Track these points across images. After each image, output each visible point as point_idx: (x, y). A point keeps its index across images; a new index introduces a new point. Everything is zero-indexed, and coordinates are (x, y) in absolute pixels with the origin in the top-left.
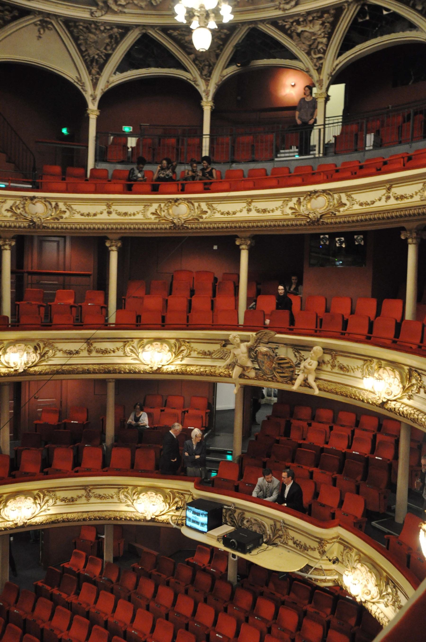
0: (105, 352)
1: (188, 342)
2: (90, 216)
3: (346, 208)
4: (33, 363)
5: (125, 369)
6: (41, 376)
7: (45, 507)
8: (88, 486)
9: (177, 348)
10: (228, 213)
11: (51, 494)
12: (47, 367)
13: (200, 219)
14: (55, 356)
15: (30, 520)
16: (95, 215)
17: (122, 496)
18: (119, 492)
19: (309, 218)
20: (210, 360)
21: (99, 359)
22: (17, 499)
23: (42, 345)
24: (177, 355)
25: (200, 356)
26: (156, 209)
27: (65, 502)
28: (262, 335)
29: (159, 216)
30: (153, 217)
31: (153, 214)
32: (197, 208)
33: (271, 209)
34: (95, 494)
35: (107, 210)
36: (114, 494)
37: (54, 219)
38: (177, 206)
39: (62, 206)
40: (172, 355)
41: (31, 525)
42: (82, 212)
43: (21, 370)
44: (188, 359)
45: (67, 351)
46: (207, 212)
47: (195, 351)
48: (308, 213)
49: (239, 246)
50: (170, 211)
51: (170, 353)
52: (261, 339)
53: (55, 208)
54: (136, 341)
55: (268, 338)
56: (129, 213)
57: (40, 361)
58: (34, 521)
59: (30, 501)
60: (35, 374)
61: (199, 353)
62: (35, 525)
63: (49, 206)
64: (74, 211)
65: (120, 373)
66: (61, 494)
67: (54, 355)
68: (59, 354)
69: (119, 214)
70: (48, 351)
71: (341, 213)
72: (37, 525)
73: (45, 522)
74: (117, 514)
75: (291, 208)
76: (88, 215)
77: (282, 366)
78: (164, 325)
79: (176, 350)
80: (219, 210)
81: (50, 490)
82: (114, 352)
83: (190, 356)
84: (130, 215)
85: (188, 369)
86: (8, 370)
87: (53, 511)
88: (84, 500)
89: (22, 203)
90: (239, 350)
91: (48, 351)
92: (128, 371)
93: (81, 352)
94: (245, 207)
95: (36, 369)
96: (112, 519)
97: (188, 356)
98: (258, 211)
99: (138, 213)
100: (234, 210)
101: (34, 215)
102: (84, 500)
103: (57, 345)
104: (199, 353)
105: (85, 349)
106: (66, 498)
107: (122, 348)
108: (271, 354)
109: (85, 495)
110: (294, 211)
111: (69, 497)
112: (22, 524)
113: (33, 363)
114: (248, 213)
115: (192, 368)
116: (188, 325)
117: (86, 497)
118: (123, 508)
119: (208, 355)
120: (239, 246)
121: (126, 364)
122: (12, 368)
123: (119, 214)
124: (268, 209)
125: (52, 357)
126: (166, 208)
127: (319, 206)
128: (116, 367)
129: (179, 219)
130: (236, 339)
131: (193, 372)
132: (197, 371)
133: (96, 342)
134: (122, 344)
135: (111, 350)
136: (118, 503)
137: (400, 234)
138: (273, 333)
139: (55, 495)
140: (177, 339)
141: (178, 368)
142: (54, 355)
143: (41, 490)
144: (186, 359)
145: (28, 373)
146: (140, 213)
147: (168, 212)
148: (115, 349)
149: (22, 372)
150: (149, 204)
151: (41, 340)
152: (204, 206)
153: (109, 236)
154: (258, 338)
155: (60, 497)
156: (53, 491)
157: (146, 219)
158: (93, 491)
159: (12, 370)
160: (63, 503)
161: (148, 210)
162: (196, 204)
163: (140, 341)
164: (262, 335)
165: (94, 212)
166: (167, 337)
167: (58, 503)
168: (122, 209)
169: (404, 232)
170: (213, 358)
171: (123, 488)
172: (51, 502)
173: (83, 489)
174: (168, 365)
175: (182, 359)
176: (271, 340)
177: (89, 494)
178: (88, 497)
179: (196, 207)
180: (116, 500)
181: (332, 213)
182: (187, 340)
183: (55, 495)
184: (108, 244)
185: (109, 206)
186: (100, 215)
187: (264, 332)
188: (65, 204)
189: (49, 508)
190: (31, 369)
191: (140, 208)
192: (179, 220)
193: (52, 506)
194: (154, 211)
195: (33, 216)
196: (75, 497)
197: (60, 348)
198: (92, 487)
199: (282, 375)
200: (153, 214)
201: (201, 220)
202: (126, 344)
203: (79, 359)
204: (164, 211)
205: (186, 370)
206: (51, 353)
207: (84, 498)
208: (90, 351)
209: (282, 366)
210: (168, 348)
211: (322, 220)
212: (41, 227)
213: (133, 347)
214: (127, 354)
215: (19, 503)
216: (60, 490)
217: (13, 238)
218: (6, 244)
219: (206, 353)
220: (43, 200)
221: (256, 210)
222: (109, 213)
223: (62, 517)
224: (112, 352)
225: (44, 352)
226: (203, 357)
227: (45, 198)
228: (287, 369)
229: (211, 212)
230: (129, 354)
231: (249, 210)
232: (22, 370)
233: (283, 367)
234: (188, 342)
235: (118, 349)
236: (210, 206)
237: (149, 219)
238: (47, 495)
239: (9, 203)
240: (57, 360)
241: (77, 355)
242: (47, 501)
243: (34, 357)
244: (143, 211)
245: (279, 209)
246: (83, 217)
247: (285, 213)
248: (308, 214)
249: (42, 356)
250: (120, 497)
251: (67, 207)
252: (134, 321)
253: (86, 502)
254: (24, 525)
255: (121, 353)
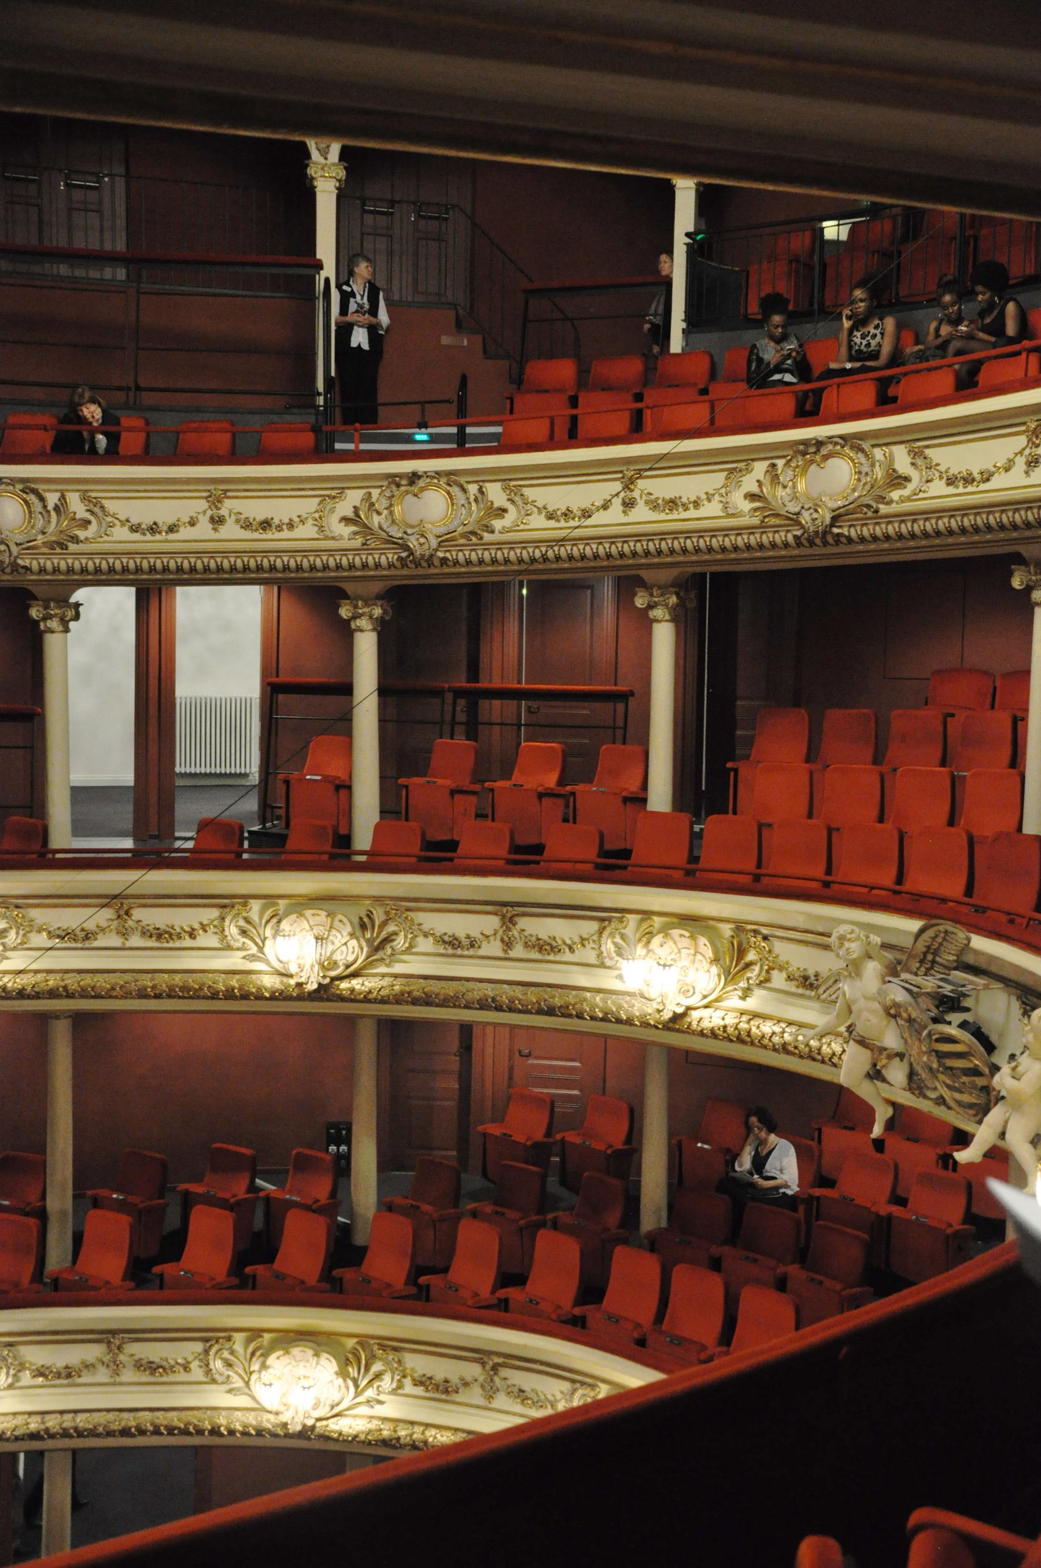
0: (546, 947)
1: (765, 938)
2: (160, 533)
3: (911, 487)
4: (348, 967)
5: (593, 1007)
6: (368, 1005)
7: (370, 1393)
8: (490, 1353)
9: (736, 957)
10: (567, 514)
11: (391, 1357)
12: (387, 981)
13: (485, 534)
14: (414, 950)
15: (324, 1423)
16: (172, 529)
17: (217, 1365)
18: (206, 1352)
19: (800, 524)
20: (816, 1005)
21: (446, 963)
22: (296, 1351)
23: (379, 916)
24: (730, 976)
25: (794, 990)
26: (355, 507)
27: (427, 1390)
28: (936, 936)
29: (366, 530)
30: (347, 530)
31: (346, 520)
32: (476, 500)
33: (693, 498)
34: (509, 1382)
35: (209, 513)
36: (559, 1396)
37: (51, 545)
38: (416, 495)
39: (76, 506)
40: (719, 976)
41: (325, 1438)
42: (134, 521)
43: (312, 986)
44: (764, 992)
45: (446, 938)
46: (505, 511)
47: (781, 969)
48: (797, 510)
49: (348, 622)
50: (397, 510)
51: (714, 970)
52: (935, 953)
53: (57, 509)
54: (255, 905)
55: (954, 949)
56: (276, 521)
57: (369, 964)
58: (335, 1427)
59: (326, 1368)
60: (352, 998)
61: (789, 978)
62: (337, 1440)
63: (37, 506)
64: (109, 519)
65: (580, 1016)
66: (418, 1363)
67: (411, 946)
68: (425, 945)
69: (247, 525)
70: (396, 934)
71: (894, 508)
72: (339, 1439)
73: (362, 1437)
74: (192, 1417)
75: (752, 497)
76: (154, 529)
77: (949, 1063)
78: (691, 876)
79: (731, 961)
80: (540, 504)
81: (393, 1346)
82: (192, 935)
83: (768, 985)
84: (279, 528)
85: (754, 1030)
86: (282, 982)
87: (392, 1408)
88: (475, 1395)
89: (388, 494)
90: (858, 983)
91: (396, 934)
92: (600, 1015)
93: (484, 944)
94: (617, 495)
95: (356, 983)
96: (206, 1433)
97: (764, 982)
98: (654, 505)
99: (303, 522)
100: (586, 504)
101: (412, 527)
102: (475, 1395)
103: (420, 917)
104: (789, 978)
105: (495, 934)
106: (430, 1378)
107: (595, 938)
108: (914, 1015)
109: (481, 1379)
110: (758, 504)
111: (439, 1377)
112: (299, 1428)
113: (348, 967)
114: (624, 512)
115: (767, 1028)
116: (827, 884)
117: (482, 1386)
118: (217, 1397)
119: (811, 987)
120: (348, 622)
121: (599, 991)
122: (291, 976)
123: (247, 525)
124: (684, 500)
125: (404, 952)
126: (385, 503)
127: (835, 481)
128: (571, 997)
129: (423, 536)
130: (847, 944)
131: (766, 1042)
132: (776, 1039)
133: (524, 915)
134: (593, 926)
135: (564, 943)
136: (205, 1383)
137: (1010, 574)
138: (961, 934)
139: (399, 1362)
140: (739, 927)
141: (731, 1020)
142: (411, 946)
143: (363, 1340)
144: (759, 993)
145: (334, 995)
146: (310, 522)
147: (391, 513)
148: (196, 926)
149: (315, 991)
150: (333, 493)
151: (378, 900)
152: (496, 494)
153: (349, 588)
154: (929, 947)
155: (413, 1369)
156: (396, 1349)
157: (326, 538)
158: (504, 1372)
159: (292, 982)
160: (420, 1391)
161: (333, 510)
162: (473, 489)
163: (642, 920)
164: (936, 936)
165: (171, 520)
166: (714, 913)
167: (409, 1388)
168: (257, 509)
169: (1023, 567)
170: (824, 1001)
171: (583, 1384)
172: (387, 1382)
173: (475, 1360)
174: (706, 1007)
175: (746, 994)
176: (970, 959)
177: (492, 1380)
178: (490, 1392)
179: (472, 498)
180: (197, 1373)
181: (869, 506)
182: (765, 931)
183: (399, 1362)
184: (34, 613)
185: (215, 501)
186: (188, 527)
187: (941, 928)
188: (85, 498)
189: (382, 1397)
190: (344, 985)
191: (309, 505)
192: (422, 540)
193: (390, 1393)
194: (349, 513)
195: (409, 531)
196: (455, 1380)
197: (426, 927)
198: (500, 1360)
199: (958, 1096)
200: (346, 520)
201: (487, 537)
202: (604, 928)
203: (473, 965)
204: (379, 513)
205: (749, 1032)
206: (400, 942)
207: (477, 1390)
208: (508, 945)
209: (949, 1063)
210: (709, 953)
211: (836, 530)
212: (437, 563)
213: (247, 920)
214: (232, 943)
215: (302, 1364)
216: (414, 1351)
217: (379, 597)
218: (360, 616)
219: (806, 978)
220: (443, 481)
221: (647, 502)
222: (217, 521)
223: (411, 1435)
224: (187, 937)
225: (384, 934)
226: (800, 991)
227: (449, 473)
228: (964, 1079)
229: (519, 512)
230: (611, 959)
231: (629, 504)
232: (315, 986)
233: (951, 1069)
234: (765, 938)
235: (204, 928)
236: (514, 493)
237: (333, 538)
238: (380, 1359)
239: (354, 497)
240: (416, 962)
241: (471, 952)
242: (378, 1376)
243: (347, 949)
244: (317, 515)
245: (717, 497)
246: (137, 536)
247: (730, 511)
248: (798, 514)
249: (378, 947)
250: (212, 1366)
251: (91, 507)
252: (680, 857)
253: (482, 1402)
254: (305, 1433)
255: (210, 940)
